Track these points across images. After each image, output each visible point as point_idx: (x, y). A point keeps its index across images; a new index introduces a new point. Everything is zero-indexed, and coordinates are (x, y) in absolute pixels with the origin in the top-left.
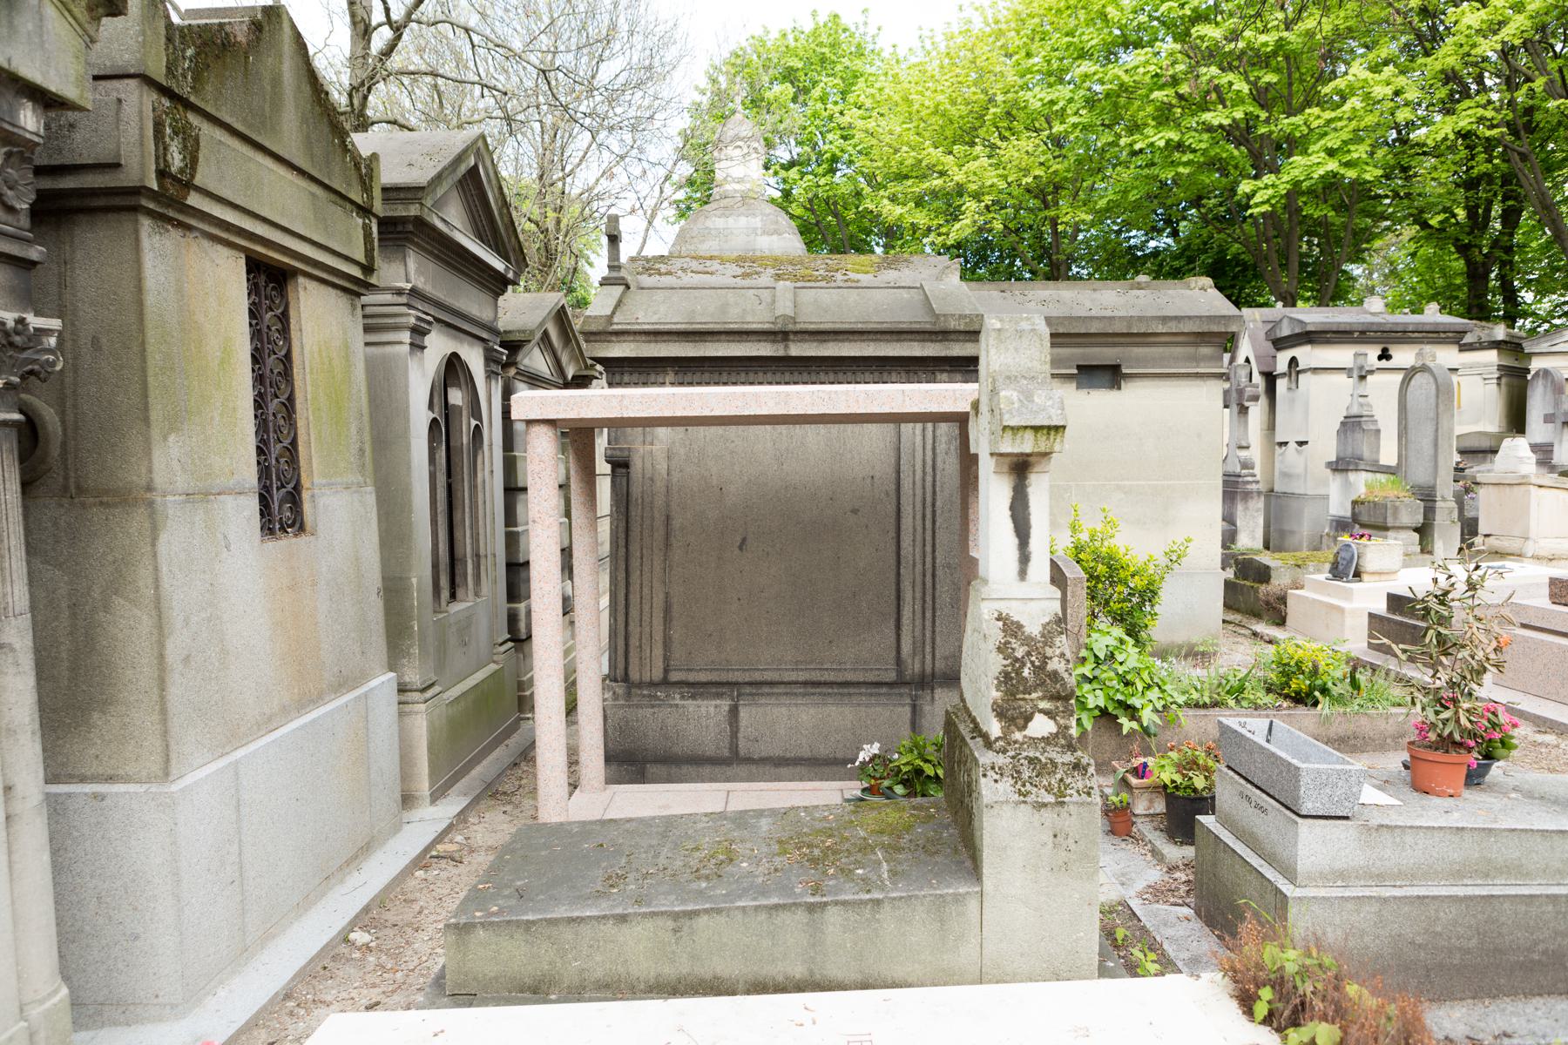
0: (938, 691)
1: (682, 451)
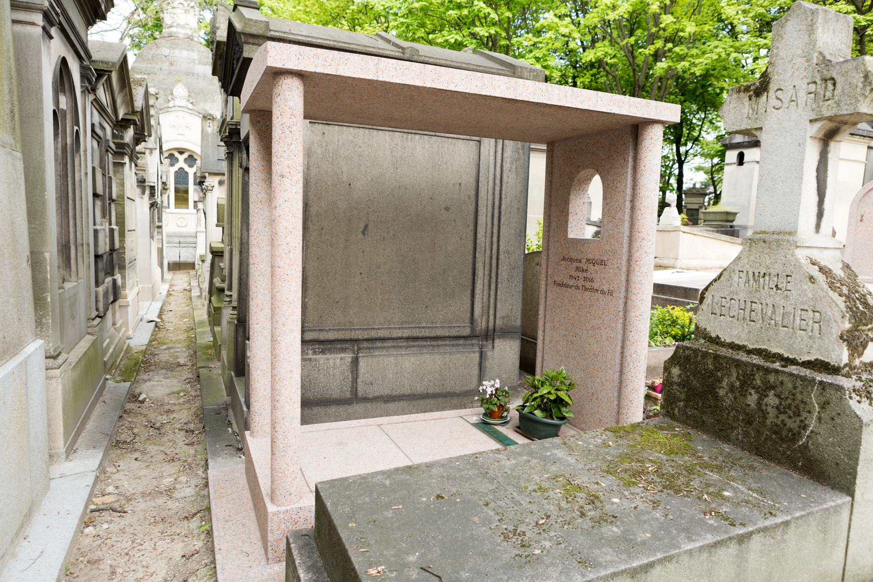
0: (497, 341)
1: (319, 151)
